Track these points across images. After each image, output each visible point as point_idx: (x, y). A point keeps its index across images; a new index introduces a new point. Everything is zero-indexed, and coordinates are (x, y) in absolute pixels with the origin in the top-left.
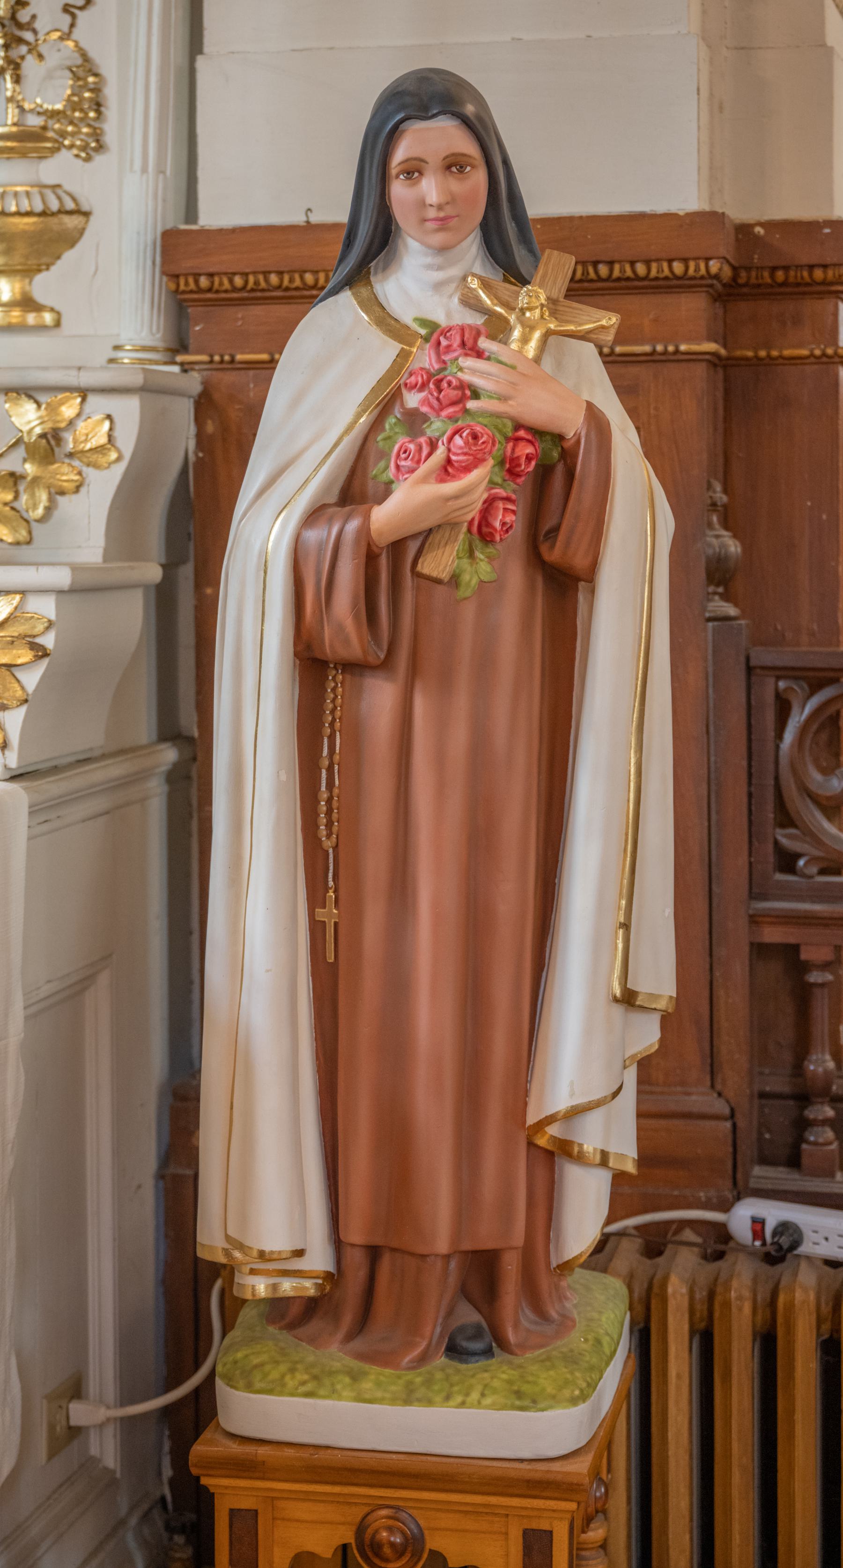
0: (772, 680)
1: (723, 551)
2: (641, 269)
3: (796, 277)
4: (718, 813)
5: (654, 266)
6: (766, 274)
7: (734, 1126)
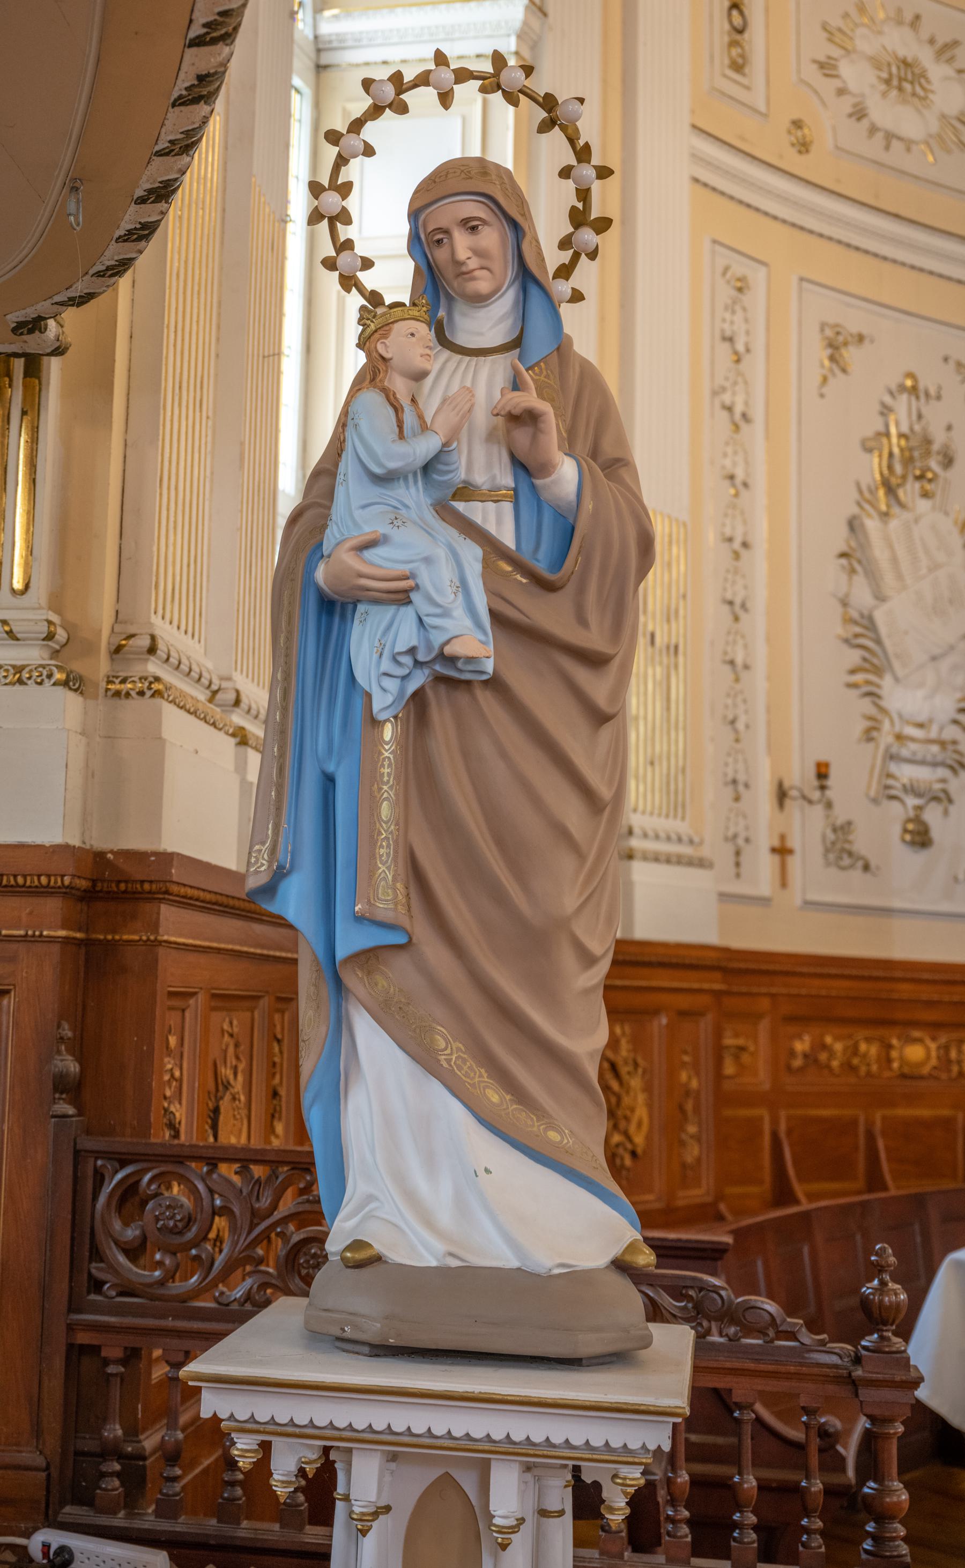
0: (92, 1160)
1: (65, 1070)
2: (44, 880)
3: (132, 888)
4: (51, 1250)
5: (29, 879)
6: (114, 885)
7: (49, 1475)
